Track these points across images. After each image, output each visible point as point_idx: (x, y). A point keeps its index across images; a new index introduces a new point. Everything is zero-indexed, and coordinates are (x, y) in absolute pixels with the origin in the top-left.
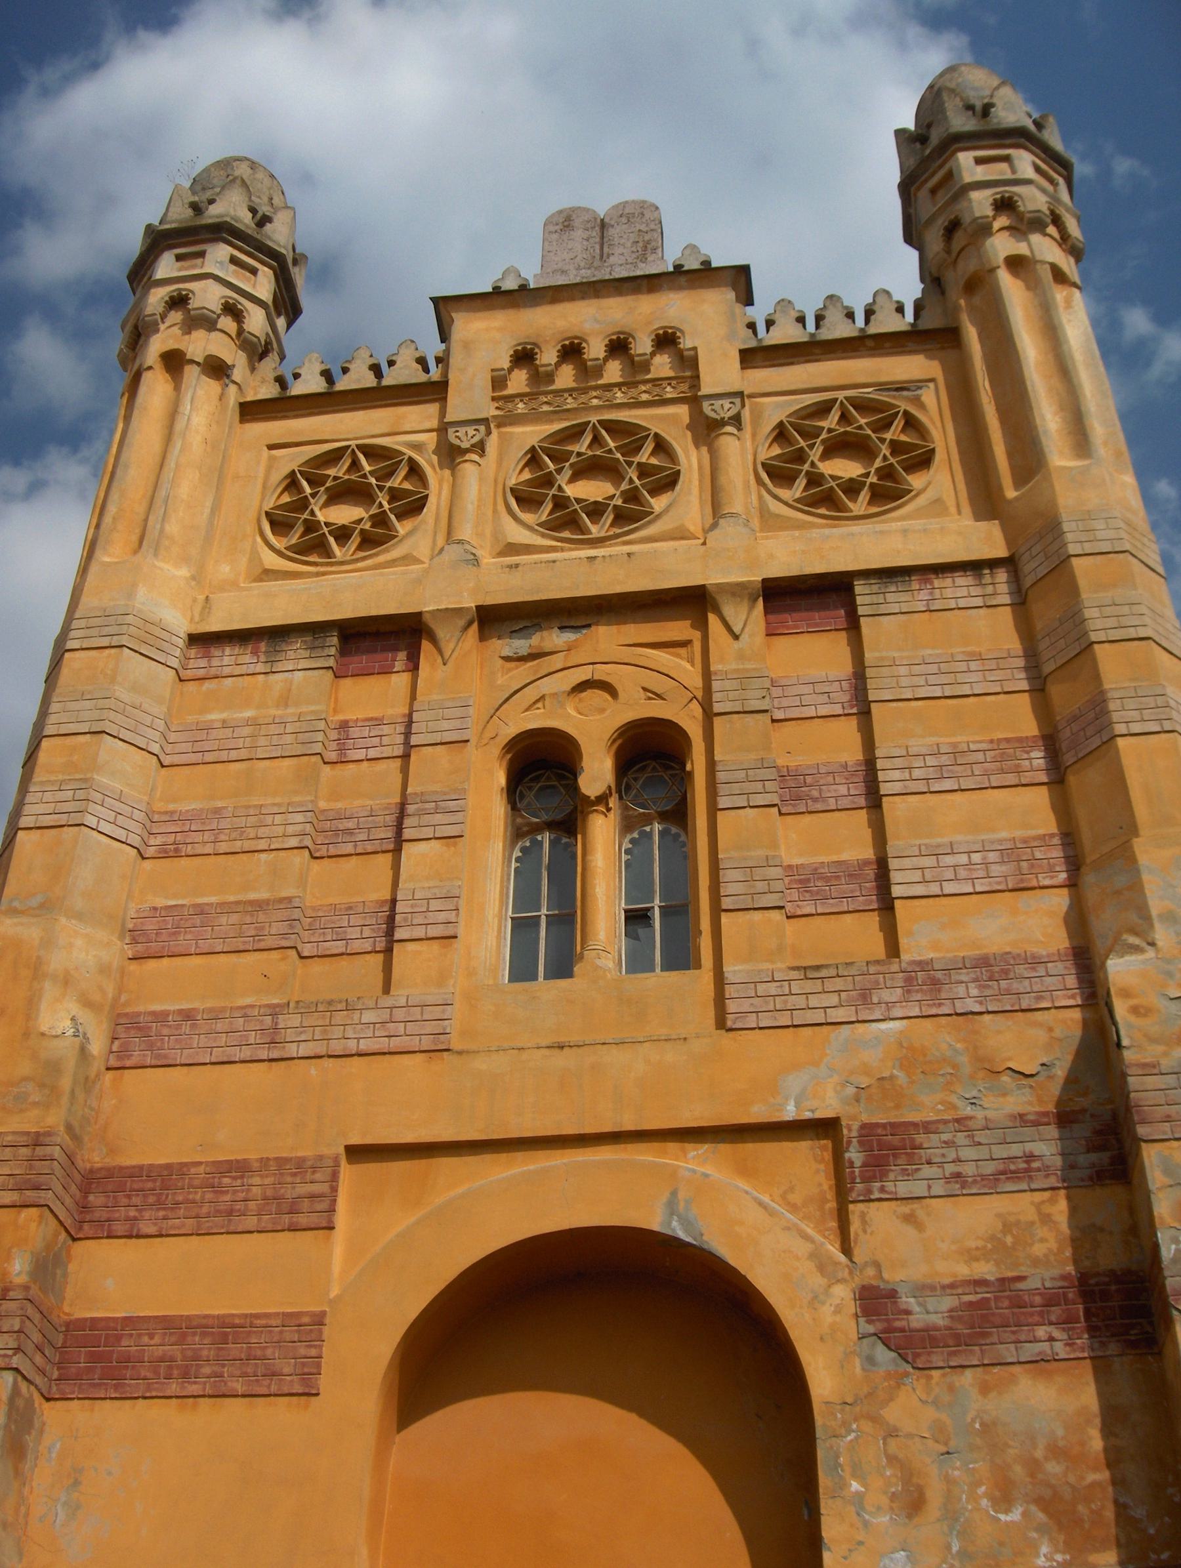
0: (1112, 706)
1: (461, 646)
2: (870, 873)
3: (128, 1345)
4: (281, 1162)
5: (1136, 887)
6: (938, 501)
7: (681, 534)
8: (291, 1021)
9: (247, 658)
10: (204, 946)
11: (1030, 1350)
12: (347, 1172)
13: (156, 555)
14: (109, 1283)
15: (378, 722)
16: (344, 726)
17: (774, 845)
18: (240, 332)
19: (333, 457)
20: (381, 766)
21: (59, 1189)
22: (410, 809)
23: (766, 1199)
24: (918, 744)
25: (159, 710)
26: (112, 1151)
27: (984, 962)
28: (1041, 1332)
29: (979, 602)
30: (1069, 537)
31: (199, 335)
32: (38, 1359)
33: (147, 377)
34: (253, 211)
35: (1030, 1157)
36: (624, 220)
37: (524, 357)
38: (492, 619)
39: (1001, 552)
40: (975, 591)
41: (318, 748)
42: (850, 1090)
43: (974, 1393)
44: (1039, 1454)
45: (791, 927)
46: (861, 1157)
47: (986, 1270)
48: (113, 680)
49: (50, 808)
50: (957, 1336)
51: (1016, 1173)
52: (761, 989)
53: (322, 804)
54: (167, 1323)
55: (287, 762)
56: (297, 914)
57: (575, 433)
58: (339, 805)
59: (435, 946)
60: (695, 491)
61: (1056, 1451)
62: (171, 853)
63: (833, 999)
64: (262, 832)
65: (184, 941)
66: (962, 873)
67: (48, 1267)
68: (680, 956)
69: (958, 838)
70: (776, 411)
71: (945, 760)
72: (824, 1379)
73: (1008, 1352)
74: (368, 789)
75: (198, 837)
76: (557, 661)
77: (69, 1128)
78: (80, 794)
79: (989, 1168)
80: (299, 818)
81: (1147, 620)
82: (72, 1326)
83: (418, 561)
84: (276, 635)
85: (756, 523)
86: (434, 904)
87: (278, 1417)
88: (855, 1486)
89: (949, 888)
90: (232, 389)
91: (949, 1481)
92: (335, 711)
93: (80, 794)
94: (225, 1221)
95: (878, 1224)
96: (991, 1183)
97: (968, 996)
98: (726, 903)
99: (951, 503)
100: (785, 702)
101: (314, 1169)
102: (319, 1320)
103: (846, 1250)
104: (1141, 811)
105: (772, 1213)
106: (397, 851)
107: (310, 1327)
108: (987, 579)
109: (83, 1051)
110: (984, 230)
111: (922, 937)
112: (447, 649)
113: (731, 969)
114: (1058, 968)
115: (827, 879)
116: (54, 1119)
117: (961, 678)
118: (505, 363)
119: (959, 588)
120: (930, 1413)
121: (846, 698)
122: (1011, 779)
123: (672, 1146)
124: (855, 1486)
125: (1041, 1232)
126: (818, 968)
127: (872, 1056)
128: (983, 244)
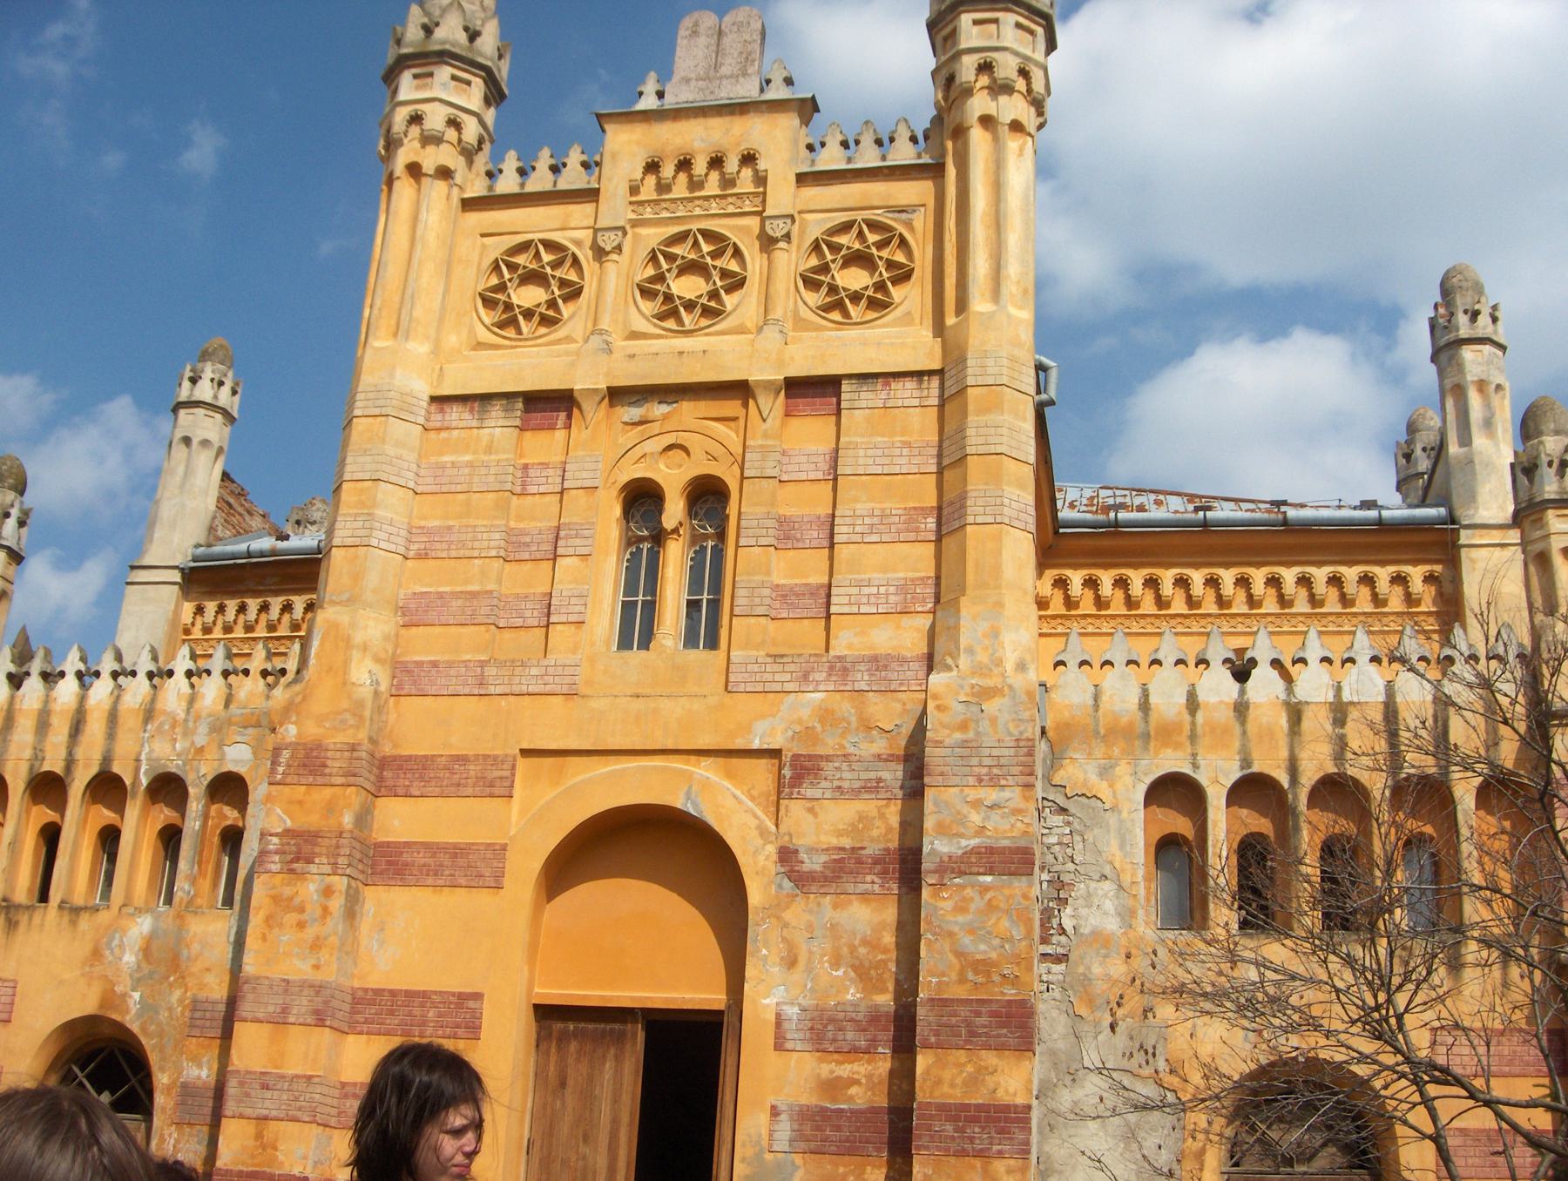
0: (969, 503)
1: (594, 412)
2: (823, 593)
3: (406, 857)
4: (486, 757)
5: (957, 628)
6: (909, 313)
7: (740, 330)
8: (491, 671)
9: (466, 415)
10: (443, 619)
11: (861, 888)
12: (522, 763)
13: (407, 338)
14: (396, 822)
15: (545, 465)
16: (526, 467)
17: (768, 573)
18: (460, 140)
19: (523, 247)
20: (547, 498)
21: (367, 774)
22: (562, 534)
23: (738, 793)
24: (862, 507)
25: (413, 457)
26: (395, 746)
27: (875, 659)
28: (869, 878)
29: (916, 402)
30: (970, 371)
31: (431, 149)
32: (360, 866)
33: (397, 185)
34: (466, 29)
35: (879, 780)
36: (735, 28)
37: (652, 167)
38: (617, 395)
39: (936, 366)
40: (916, 393)
41: (508, 486)
42: (790, 733)
43: (829, 907)
44: (857, 943)
45: (772, 625)
46: (794, 772)
47: (846, 842)
48: (383, 441)
49: (349, 533)
50: (826, 877)
51: (873, 788)
52: (750, 667)
53: (512, 524)
54: (426, 846)
55: (491, 495)
56: (495, 602)
57: (680, 238)
58: (522, 525)
59: (573, 627)
60: (755, 293)
61: (865, 942)
62: (422, 556)
63: (788, 677)
64: (477, 544)
65: (432, 616)
66: (873, 600)
67: (363, 818)
68: (712, 644)
69: (875, 575)
70: (816, 226)
71: (876, 520)
72: (756, 895)
73: (850, 888)
74: (536, 515)
75: (438, 546)
76: (655, 428)
77: (371, 739)
78: (367, 524)
79: (857, 785)
80: (497, 536)
81: (1005, 439)
82: (378, 845)
83: (575, 341)
84: (481, 400)
85: (789, 325)
86: (573, 601)
87: (483, 899)
88: (764, 951)
89: (864, 609)
90: (455, 190)
91: (810, 952)
92: (521, 456)
93: (367, 524)
94: (455, 789)
95: (795, 810)
96: (856, 793)
97: (862, 680)
98: (737, 611)
99: (917, 317)
100: (790, 468)
101: (503, 762)
102: (504, 848)
103: (777, 826)
104: (971, 577)
105: (740, 802)
106: (555, 560)
107: (499, 851)
108: (925, 385)
109: (376, 693)
110: (968, 92)
111: (845, 641)
112: (589, 416)
113: (736, 655)
114: (915, 666)
115: (797, 595)
116: (362, 735)
117: (896, 460)
118: (639, 175)
119: (905, 391)
120: (807, 917)
121: (826, 467)
122: (912, 536)
123: (693, 758)
124: (764, 951)
125: (878, 823)
126: (782, 656)
127: (805, 713)
128: (964, 103)
